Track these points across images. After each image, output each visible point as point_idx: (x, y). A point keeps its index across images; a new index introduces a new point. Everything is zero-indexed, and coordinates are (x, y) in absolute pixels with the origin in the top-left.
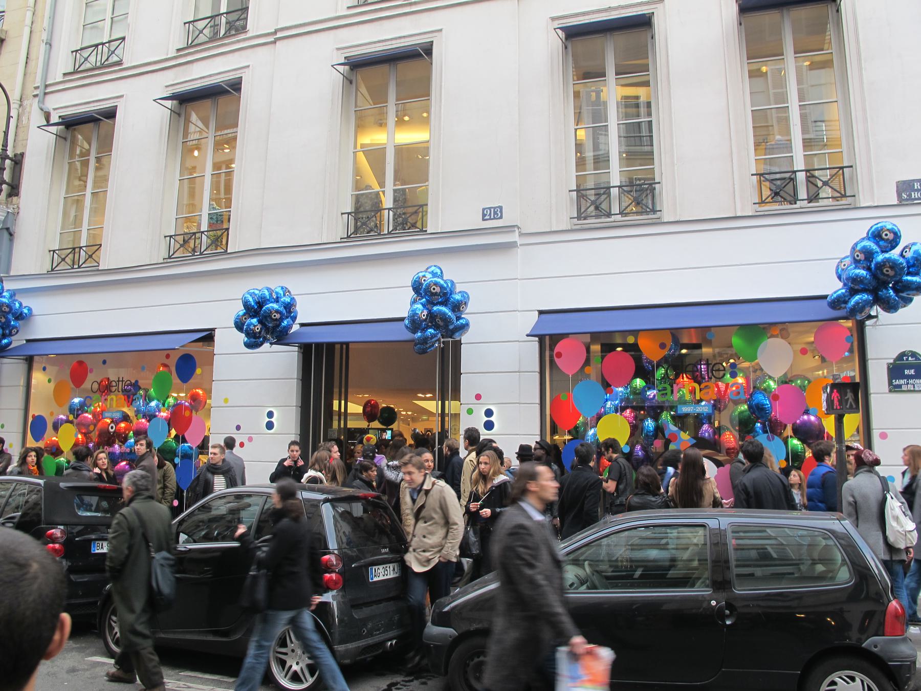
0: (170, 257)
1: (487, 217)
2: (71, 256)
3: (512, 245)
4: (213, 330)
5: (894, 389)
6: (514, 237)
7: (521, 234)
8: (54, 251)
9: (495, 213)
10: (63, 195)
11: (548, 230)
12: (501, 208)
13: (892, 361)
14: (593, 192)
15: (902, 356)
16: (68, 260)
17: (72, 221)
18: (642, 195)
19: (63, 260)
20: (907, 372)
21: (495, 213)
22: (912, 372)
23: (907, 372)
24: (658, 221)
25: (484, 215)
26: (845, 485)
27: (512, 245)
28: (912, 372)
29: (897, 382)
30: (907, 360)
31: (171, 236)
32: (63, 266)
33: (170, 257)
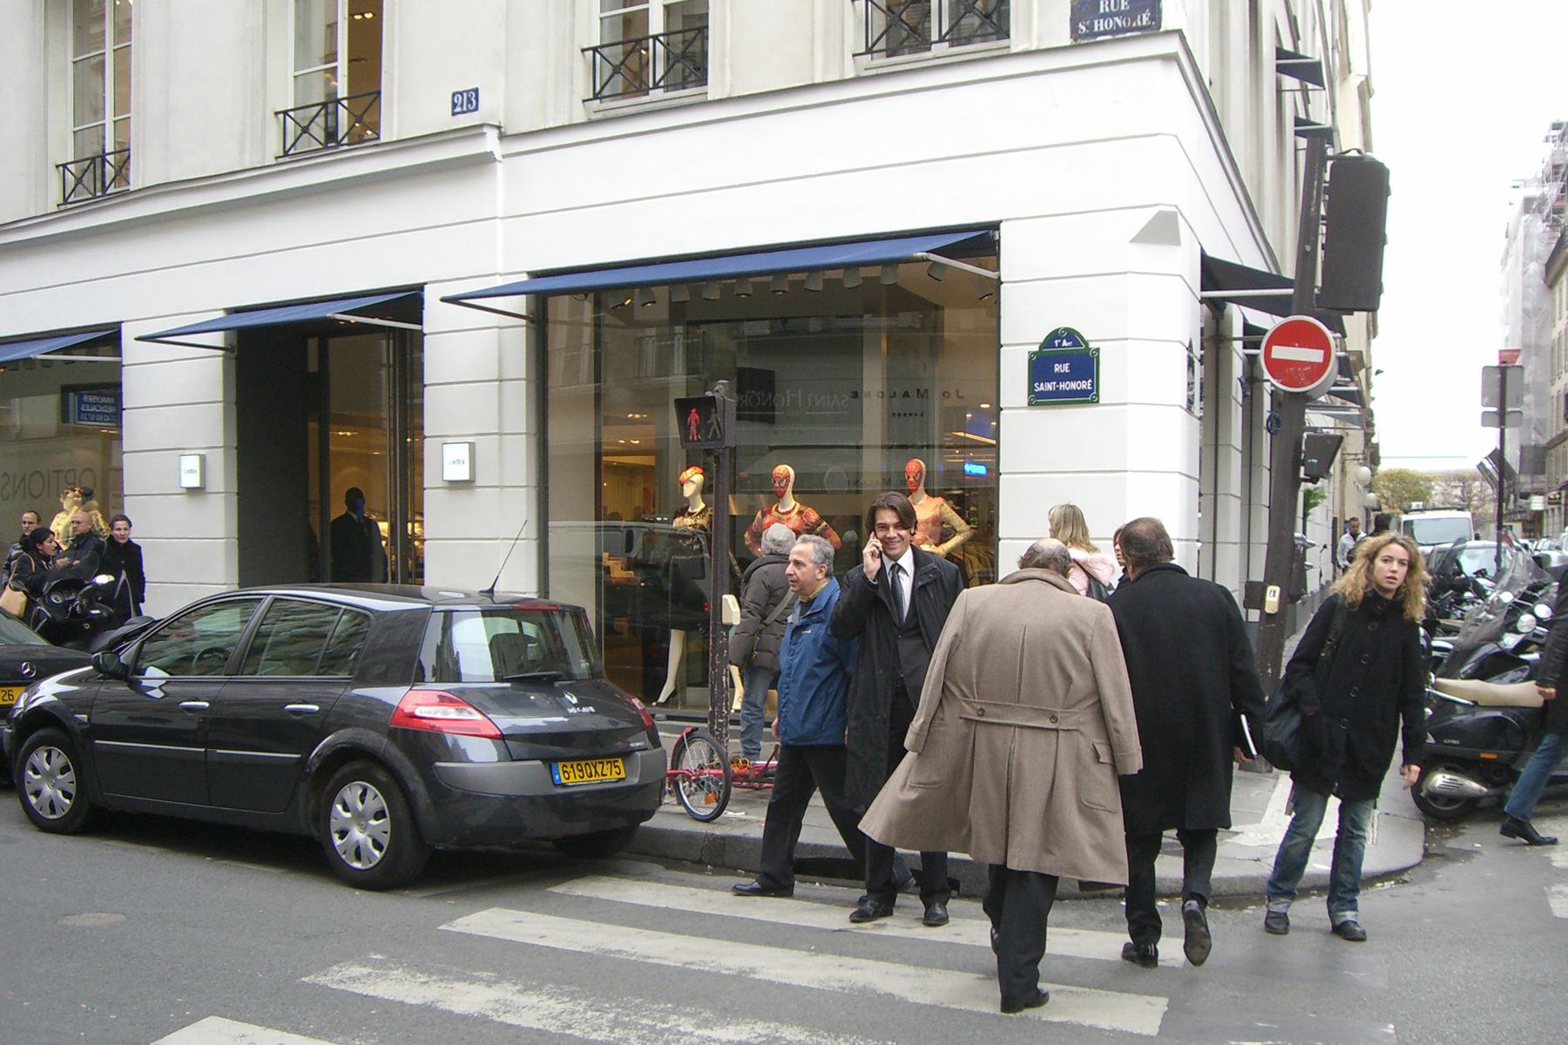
0: (596, 97)
1: (458, 109)
2: (321, 120)
3: (486, 159)
4: (995, 226)
5: (1037, 399)
6: (490, 143)
7: (503, 137)
8: (285, 113)
9: (469, 102)
10: (71, 58)
11: (837, 78)
12: (476, 91)
13: (1036, 348)
14: (680, 37)
15: (1055, 335)
16: (318, 130)
17: (87, 104)
18: (690, 62)
19: (305, 130)
20: (1057, 368)
21: (467, 100)
22: (1065, 368)
23: (1057, 368)
24: (1005, 52)
25: (454, 105)
26: (1193, 574)
27: (484, 161)
28: (1065, 368)
29: (1042, 388)
30: (1060, 345)
31: (595, 49)
32: (306, 144)
33: (286, 154)
